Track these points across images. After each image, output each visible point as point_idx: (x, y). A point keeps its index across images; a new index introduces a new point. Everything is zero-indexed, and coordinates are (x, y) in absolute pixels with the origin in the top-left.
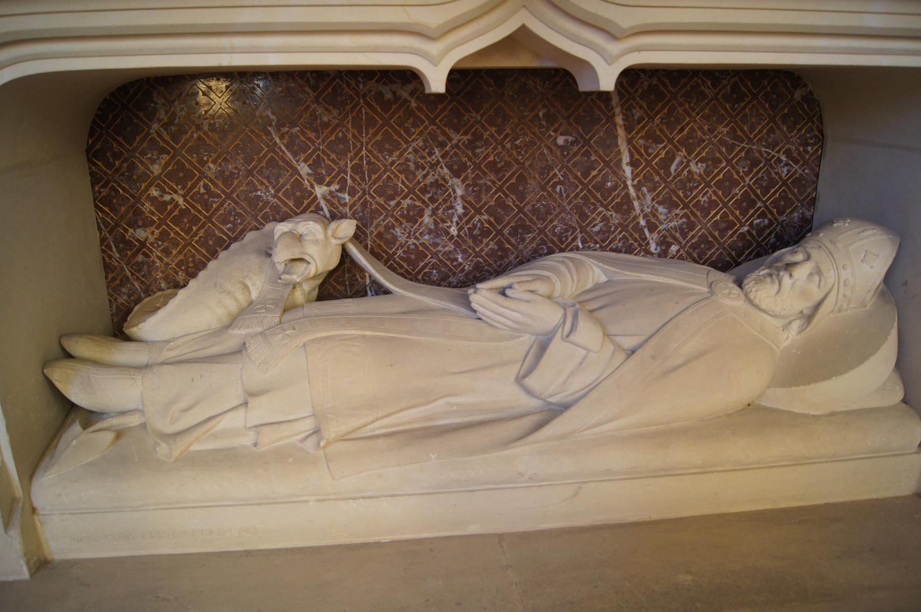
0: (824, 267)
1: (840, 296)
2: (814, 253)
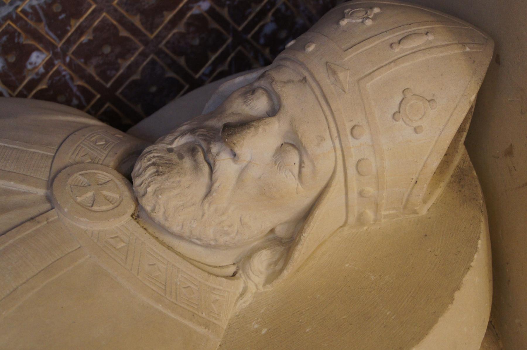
0: (308, 135)
1: (354, 195)
2: (291, 97)
